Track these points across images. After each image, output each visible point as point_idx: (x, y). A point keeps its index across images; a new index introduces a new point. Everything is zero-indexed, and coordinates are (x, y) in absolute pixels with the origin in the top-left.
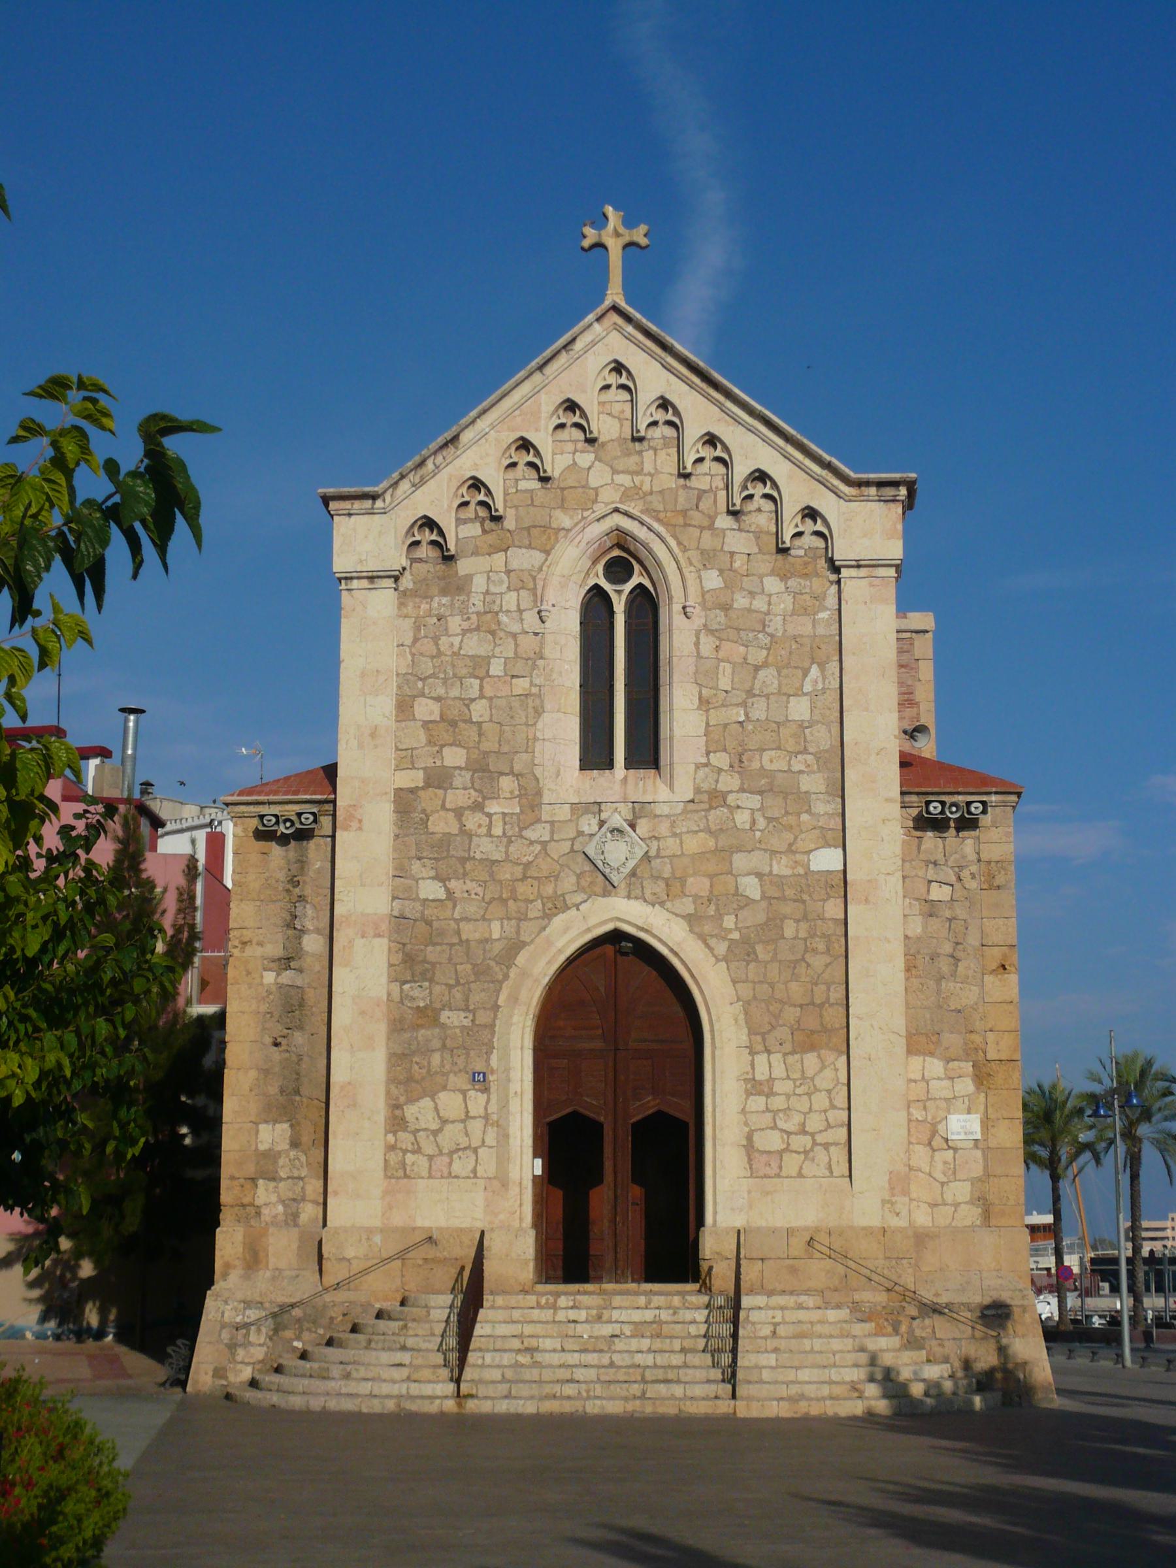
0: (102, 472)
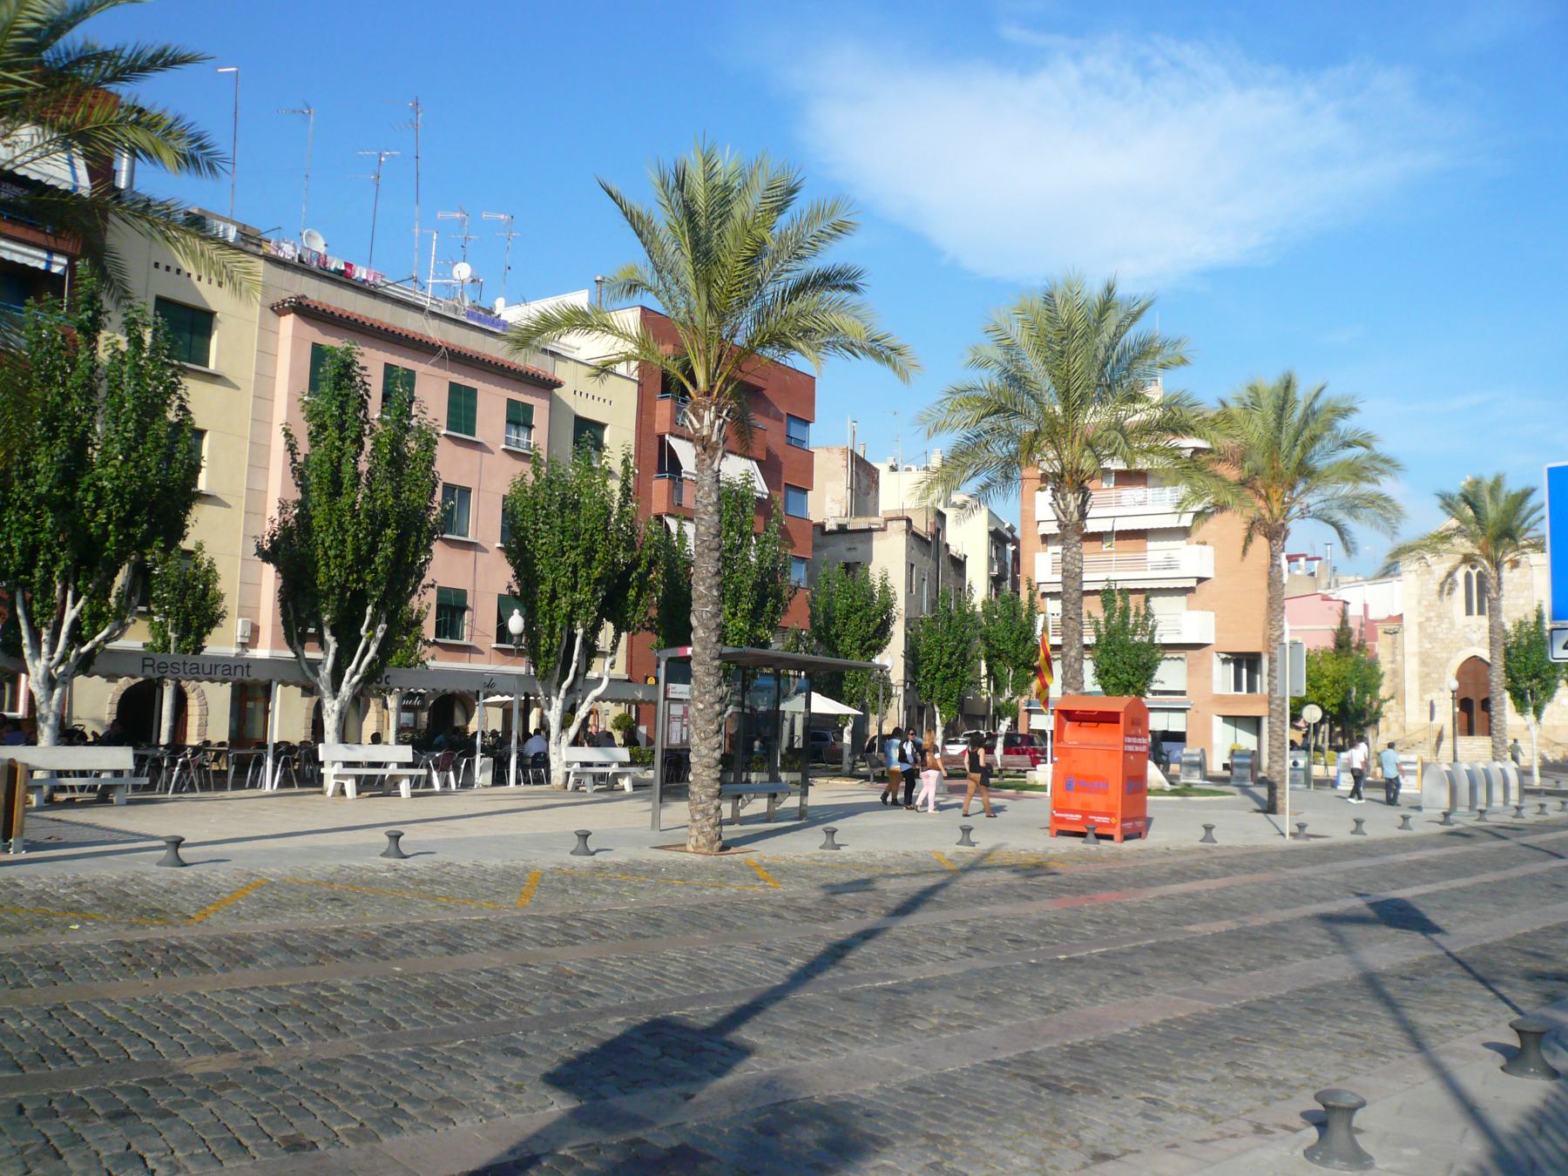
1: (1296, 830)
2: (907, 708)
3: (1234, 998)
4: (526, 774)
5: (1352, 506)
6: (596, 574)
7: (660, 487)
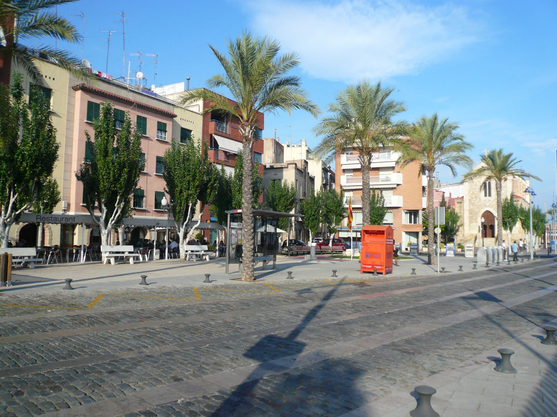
0: (458, 238)
1: (441, 270)
2: (296, 230)
3: (448, 324)
4: (170, 255)
5: (457, 160)
6: (197, 184)
7: (211, 153)
